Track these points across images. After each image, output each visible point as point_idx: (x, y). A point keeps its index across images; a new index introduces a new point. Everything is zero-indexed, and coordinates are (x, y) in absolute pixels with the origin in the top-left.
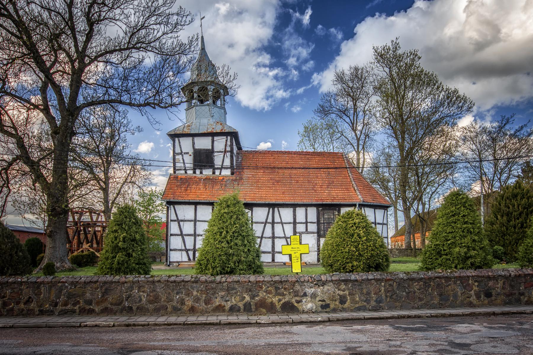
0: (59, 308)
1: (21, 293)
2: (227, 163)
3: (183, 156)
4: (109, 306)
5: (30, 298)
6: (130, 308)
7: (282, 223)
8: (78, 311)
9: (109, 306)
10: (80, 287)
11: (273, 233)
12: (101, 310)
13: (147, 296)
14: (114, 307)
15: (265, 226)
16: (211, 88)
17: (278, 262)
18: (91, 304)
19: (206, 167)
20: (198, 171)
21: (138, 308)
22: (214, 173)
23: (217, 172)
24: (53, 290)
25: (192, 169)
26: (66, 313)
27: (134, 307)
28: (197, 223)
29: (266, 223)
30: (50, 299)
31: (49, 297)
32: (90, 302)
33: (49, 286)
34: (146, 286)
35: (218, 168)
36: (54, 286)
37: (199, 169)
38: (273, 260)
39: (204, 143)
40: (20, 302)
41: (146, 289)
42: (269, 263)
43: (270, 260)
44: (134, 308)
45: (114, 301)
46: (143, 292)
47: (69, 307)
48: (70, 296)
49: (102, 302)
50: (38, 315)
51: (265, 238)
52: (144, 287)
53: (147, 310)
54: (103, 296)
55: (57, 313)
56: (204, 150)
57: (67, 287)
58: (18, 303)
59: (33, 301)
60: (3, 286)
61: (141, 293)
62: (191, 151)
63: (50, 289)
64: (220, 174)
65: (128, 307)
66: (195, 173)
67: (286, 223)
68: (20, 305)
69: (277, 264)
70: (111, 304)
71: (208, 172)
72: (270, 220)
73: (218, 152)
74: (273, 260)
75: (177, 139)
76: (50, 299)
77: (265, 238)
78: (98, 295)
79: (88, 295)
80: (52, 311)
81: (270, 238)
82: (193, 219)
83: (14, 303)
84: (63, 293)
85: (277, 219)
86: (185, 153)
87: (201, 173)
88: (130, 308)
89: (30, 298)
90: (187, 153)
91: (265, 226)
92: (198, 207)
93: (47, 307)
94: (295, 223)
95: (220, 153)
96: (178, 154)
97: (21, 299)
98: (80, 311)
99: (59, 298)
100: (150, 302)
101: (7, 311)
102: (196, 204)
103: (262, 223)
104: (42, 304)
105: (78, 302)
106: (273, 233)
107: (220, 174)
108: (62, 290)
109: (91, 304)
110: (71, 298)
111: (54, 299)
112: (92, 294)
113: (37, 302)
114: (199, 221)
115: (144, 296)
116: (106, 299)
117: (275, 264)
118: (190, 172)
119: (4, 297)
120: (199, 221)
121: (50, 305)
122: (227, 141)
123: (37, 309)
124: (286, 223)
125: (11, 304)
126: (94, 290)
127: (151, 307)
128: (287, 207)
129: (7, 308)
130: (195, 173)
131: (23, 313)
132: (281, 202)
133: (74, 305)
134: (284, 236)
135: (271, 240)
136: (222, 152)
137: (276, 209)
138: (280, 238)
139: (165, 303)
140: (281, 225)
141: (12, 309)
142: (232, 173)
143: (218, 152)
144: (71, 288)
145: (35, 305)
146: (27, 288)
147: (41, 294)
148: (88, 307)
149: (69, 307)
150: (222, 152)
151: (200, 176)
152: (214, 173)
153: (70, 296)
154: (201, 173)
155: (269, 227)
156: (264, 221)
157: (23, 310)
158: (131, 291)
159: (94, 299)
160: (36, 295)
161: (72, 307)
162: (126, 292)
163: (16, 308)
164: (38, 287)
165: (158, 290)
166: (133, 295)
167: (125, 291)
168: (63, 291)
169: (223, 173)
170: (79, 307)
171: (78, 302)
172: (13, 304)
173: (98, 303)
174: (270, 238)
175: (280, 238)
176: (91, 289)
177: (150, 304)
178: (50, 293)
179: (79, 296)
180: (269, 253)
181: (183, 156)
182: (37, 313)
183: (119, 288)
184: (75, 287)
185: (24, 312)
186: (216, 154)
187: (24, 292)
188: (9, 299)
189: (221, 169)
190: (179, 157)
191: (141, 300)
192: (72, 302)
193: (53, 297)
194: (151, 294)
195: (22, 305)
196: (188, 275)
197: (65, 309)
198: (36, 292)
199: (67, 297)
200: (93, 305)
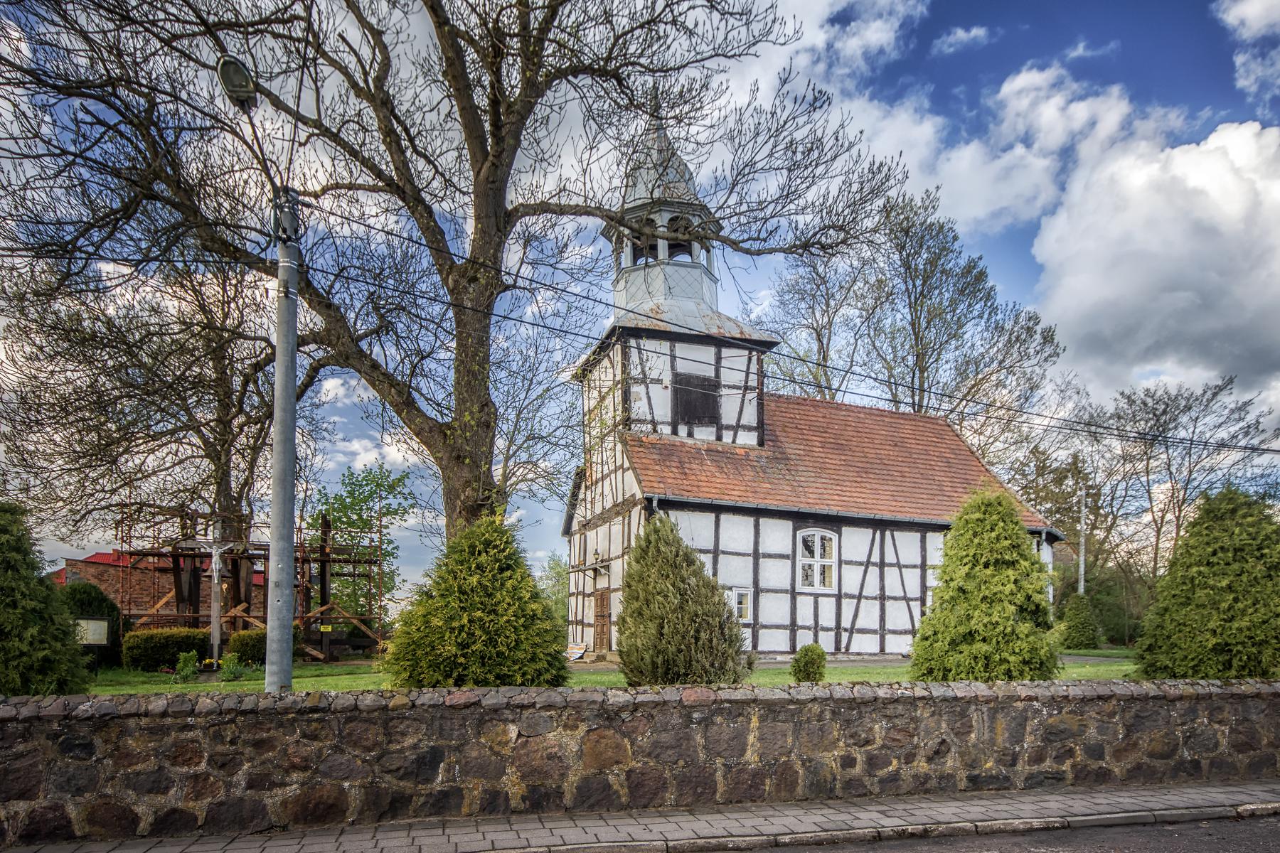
0: (1022, 768)
1: (915, 729)
2: (750, 417)
3: (647, 387)
4: (1145, 759)
5: (944, 741)
6: (1196, 764)
7: (899, 566)
8: (1070, 776)
9: (1145, 759)
10: (1070, 712)
11: (882, 588)
12: (1128, 771)
13: (1232, 730)
14: (1158, 764)
15: (866, 572)
16: (662, 219)
17: (858, 654)
18: (1101, 757)
19: (701, 422)
20: (683, 430)
21: (1212, 764)
22: (719, 438)
23: (727, 437)
24: (1002, 722)
25: (668, 423)
26: (1040, 784)
27: (1203, 762)
28: (721, 557)
29: (868, 564)
30: (994, 745)
31: (992, 742)
32: (1096, 752)
33: (989, 709)
34: (1227, 707)
35: (728, 428)
36: (1003, 708)
37: (686, 423)
38: (882, 649)
39: (697, 361)
40: (914, 755)
41: (1226, 714)
42: (875, 655)
43: (876, 649)
44: (1205, 764)
45: (1158, 747)
46: (1219, 722)
47: (1048, 765)
48: (1050, 735)
49: (1126, 750)
50: (909, 793)
51: (867, 598)
52: (1220, 709)
53: (1233, 768)
54: (1126, 736)
55: (1020, 784)
56: (698, 377)
57: (1038, 712)
58: (910, 758)
59: (949, 750)
60: (863, 709)
61: (1217, 726)
62: (667, 378)
63: (993, 718)
64: (734, 442)
65: (1191, 761)
66: (675, 432)
67: (906, 567)
68: (915, 764)
69: (890, 657)
70: (1151, 755)
71: (704, 434)
72: (876, 558)
73: (730, 387)
74: (882, 649)
75: (633, 342)
76: (994, 745)
77: (867, 598)
78: (1116, 733)
79: (1092, 731)
80: (1007, 779)
81: (875, 598)
82: (711, 547)
83: (898, 758)
84: (1028, 729)
85: (890, 557)
86: (653, 381)
87: (690, 435)
88: (1196, 764)
89: (944, 741)
90: (659, 381)
91: (866, 572)
92: (724, 517)
93: (991, 769)
94: (923, 567)
95: (735, 391)
96: (636, 381)
97: (917, 747)
98: (1076, 777)
99: (1020, 741)
100: (1239, 747)
101: (882, 781)
102: (718, 509)
103: (860, 564)
104: (974, 761)
105: (1070, 753)
106: (882, 588)
107: (734, 442)
108: (1026, 719)
109: (1101, 757)
110: (1051, 742)
111: (1007, 745)
112: (1100, 730)
113: (962, 754)
114: (724, 552)
115: (1223, 732)
116: (1135, 744)
117: (852, 658)
118: (667, 430)
119: (867, 742)
120: (724, 552)
121: (998, 761)
122: (750, 359)
123: (962, 774)
124: (906, 567)
125: (891, 763)
126: (1105, 718)
127: (1242, 759)
128: (910, 530)
129: (880, 773)
130: (675, 432)
131: (928, 786)
132: (900, 517)
133: (1059, 759)
134: (902, 594)
135: (877, 603)
136: (738, 388)
137: (888, 533)
138: (895, 598)
139: (1271, 750)
140: (896, 569)
141: (895, 777)
142: (761, 443)
143: (730, 387)
144: (1050, 715)
145: (958, 765)
146: (933, 714)
147: (970, 732)
148: (1094, 765)
149: (1048, 765)
150: (738, 388)
151: (690, 441)
152: (719, 438)
153: (1050, 735)
154: (690, 435)
155: (874, 572)
156: (865, 559)
157: (927, 778)
158: (1193, 721)
159: (1108, 742)
160: (956, 734)
161: (1055, 766)
162: (1183, 724)
163: (906, 773)
164: (963, 714)
165: (1254, 717)
166: (1199, 731)
167: (1179, 721)
168: (1029, 723)
169: (740, 441)
170: (1073, 766)
171: (1070, 753)
172: (895, 762)
173: (1118, 754)
174: (875, 598)
175: (895, 598)
176: (1098, 717)
177: (1240, 752)
178: (992, 729)
179: (1073, 735)
180: (874, 632)
181: (647, 387)
182: (963, 784)
183: (1163, 713)
184: (1060, 712)
185: (933, 783)
186: (724, 391)
187: (923, 726)
188: (883, 746)
189: (736, 428)
190: (637, 389)
191: (1217, 745)
192: (1054, 753)
193: (1002, 738)
194: (1240, 728)
195: (923, 764)
196: (903, 682)
197: (1040, 773)
198: (958, 725)
199: (1043, 741)
200: (1108, 758)
